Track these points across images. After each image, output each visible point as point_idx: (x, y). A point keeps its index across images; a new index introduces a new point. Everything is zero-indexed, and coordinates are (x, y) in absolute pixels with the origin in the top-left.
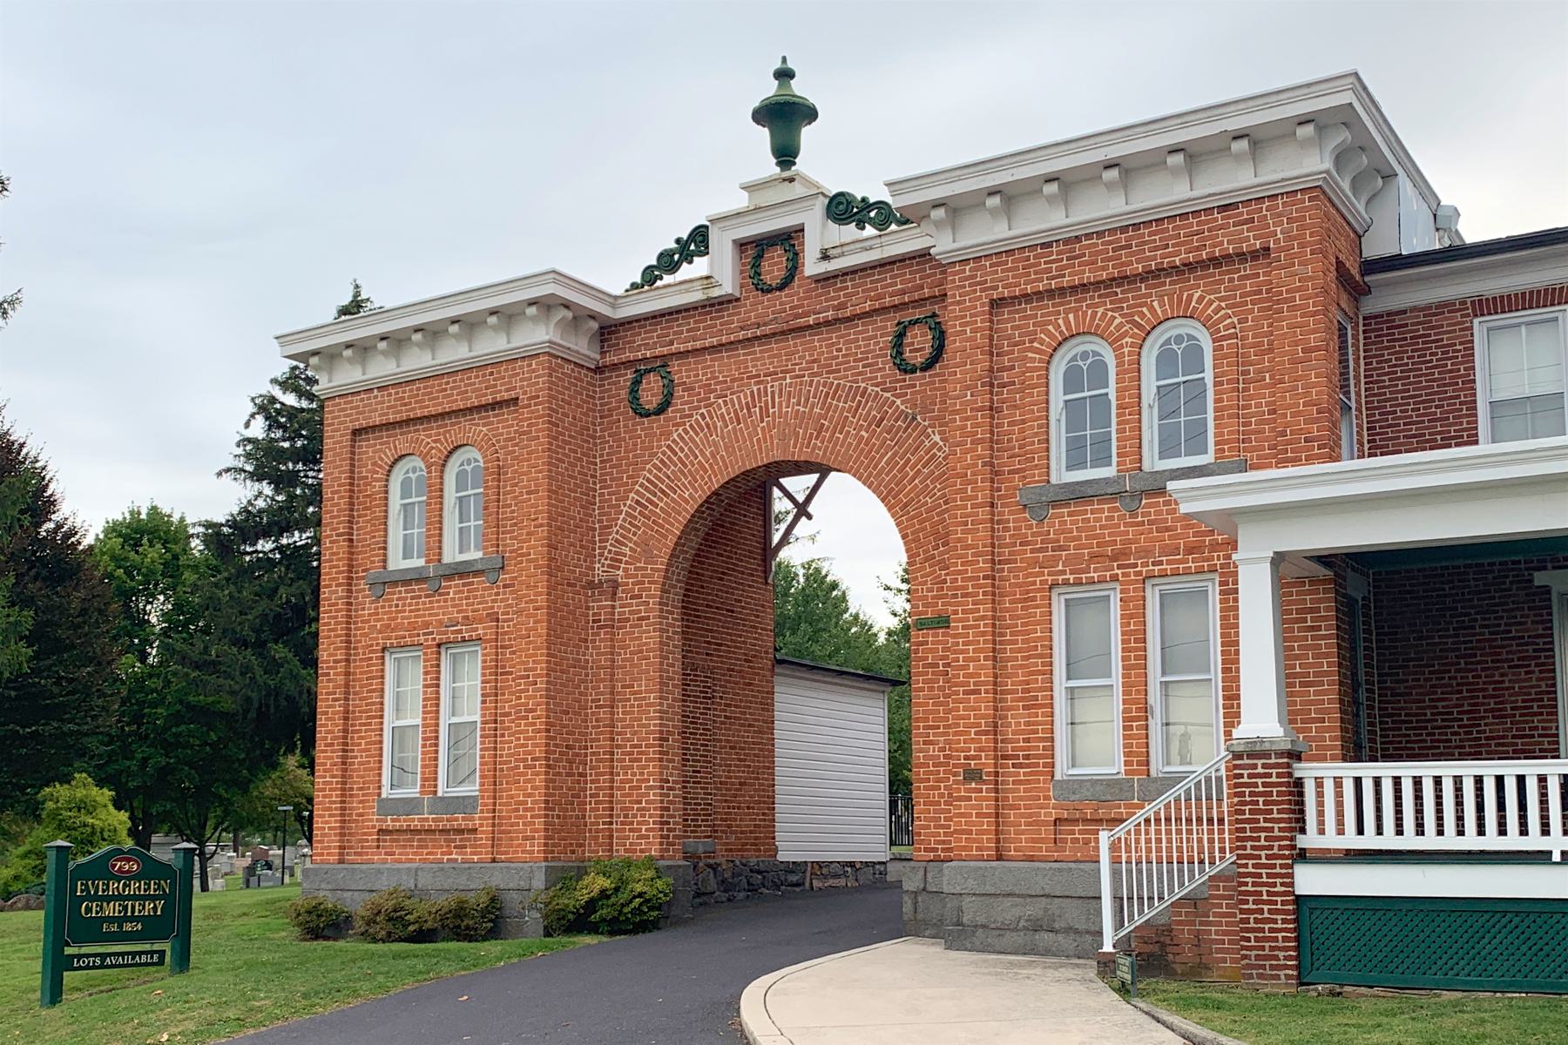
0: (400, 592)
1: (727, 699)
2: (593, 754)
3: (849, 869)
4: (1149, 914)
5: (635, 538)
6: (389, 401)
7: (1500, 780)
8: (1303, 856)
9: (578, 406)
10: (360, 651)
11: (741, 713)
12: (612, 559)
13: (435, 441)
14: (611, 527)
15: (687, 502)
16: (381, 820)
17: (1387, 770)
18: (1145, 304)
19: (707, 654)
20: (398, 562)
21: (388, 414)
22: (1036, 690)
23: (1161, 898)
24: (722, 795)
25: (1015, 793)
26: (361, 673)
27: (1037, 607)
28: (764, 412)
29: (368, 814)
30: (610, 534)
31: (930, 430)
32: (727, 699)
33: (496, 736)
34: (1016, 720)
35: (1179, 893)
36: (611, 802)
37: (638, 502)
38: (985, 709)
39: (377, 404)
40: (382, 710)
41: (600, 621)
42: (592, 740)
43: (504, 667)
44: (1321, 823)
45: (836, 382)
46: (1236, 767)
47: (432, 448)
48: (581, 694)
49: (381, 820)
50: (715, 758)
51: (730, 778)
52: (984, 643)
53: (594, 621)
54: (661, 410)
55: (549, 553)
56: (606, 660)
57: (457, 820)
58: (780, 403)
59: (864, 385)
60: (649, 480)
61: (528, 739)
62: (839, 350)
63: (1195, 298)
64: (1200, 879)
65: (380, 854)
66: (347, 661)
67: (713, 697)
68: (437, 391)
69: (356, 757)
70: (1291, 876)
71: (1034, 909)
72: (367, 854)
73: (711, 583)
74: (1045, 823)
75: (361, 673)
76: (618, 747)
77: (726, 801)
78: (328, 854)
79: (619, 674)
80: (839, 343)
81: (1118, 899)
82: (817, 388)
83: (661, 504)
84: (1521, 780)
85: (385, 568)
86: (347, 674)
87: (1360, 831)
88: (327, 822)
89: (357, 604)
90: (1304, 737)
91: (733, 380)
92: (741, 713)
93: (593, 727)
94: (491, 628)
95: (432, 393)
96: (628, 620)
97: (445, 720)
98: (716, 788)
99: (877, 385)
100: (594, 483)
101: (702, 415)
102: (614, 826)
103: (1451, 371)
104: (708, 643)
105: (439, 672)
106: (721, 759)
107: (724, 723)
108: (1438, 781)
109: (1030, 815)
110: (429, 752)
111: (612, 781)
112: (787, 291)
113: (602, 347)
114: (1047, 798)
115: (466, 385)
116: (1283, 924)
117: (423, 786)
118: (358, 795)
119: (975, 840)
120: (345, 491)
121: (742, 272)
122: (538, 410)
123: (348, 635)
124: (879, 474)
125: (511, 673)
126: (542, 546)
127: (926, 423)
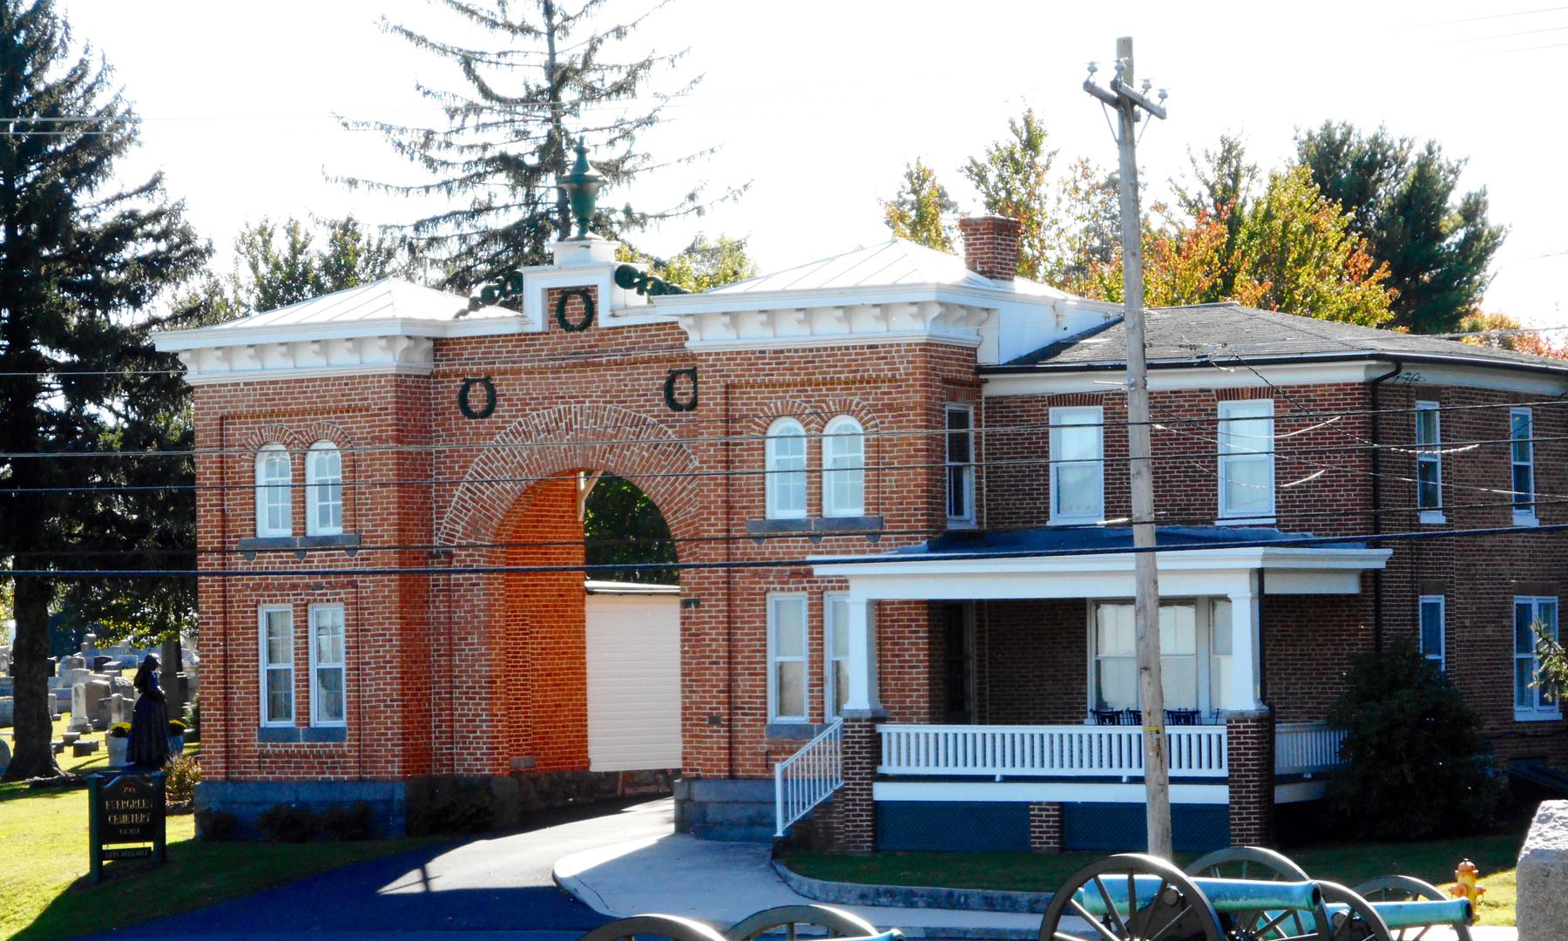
0: (270, 557)
1: (542, 632)
2: (437, 693)
3: (661, 776)
4: (803, 813)
5: (466, 519)
6: (255, 395)
7: (1003, 736)
8: (885, 778)
9: (417, 409)
10: (236, 605)
11: (555, 643)
12: (447, 534)
13: (297, 432)
14: (446, 507)
15: (508, 493)
16: (261, 746)
17: (942, 729)
18: (824, 401)
19: (525, 596)
20: (265, 531)
21: (254, 406)
22: (756, 663)
23: (809, 803)
24: (540, 717)
25: (743, 732)
26: (237, 623)
27: (757, 605)
28: (569, 428)
29: (250, 741)
30: (445, 513)
31: (692, 457)
32: (542, 632)
33: (358, 680)
34: (743, 682)
35: (819, 800)
36: (452, 732)
37: (468, 489)
38: (723, 674)
39: (244, 396)
40: (257, 655)
41: (438, 585)
42: (435, 682)
43: (363, 625)
44: (918, 760)
45: (624, 410)
46: (846, 727)
47: (295, 439)
48: (426, 645)
49: (261, 746)
50: (533, 686)
51: (547, 701)
52: (722, 629)
53: (434, 586)
54: (487, 413)
55: (399, 536)
56: (445, 618)
57: (328, 746)
58: (581, 421)
59: (644, 415)
60: (476, 472)
61: (385, 687)
62: (626, 385)
63: (854, 403)
64: (830, 792)
65: (262, 773)
66: (225, 613)
67: (532, 632)
68: (299, 393)
69: (236, 693)
70: (871, 790)
71: (751, 811)
72: (250, 773)
73: (527, 532)
74: (761, 754)
75: (237, 623)
76: (457, 687)
77: (543, 722)
78: (215, 773)
79: (455, 629)
80: (625, 380)
81: (786, 803)
82: (610, 413)
83: (487, 493)
84: (956, 735)
85: (255, 535)
86: (225, 623)
87: (937, 764)
88: (213, 747)
89: (230, 564)
90: (1436, 606)
91: (544, 398)
92: (555, 643)
93: (436, 671)
94: (352, 593)
95: (293, 393)
96: (462, 585)
97: (314, 667)
98: (534, 712)
99: (654, 417)
100: (431, 470)
101: (520, 423)
102: (455, 751)
103: (1034, 443)
104: (526, 586)
105: (307, 627)
106: (539, 686)
107: (540, 654)
108: (956, 735)
109: (752, 749)
110: (301, 692)
111: (452, 715)
112: (585, 332)
113: (435, 356)
114: (762, 737)
115: (324, 391)
116: (865, 821)
117: (298, 719)
118: (239, 725)
119: (715, 766)
120: (217, 468)
121: (550, 311)
122: (387, 420)
123: (224, 591)
124: (657, 486)
125: (369, 630)
126: (394, 530)
127: (690, 451)
